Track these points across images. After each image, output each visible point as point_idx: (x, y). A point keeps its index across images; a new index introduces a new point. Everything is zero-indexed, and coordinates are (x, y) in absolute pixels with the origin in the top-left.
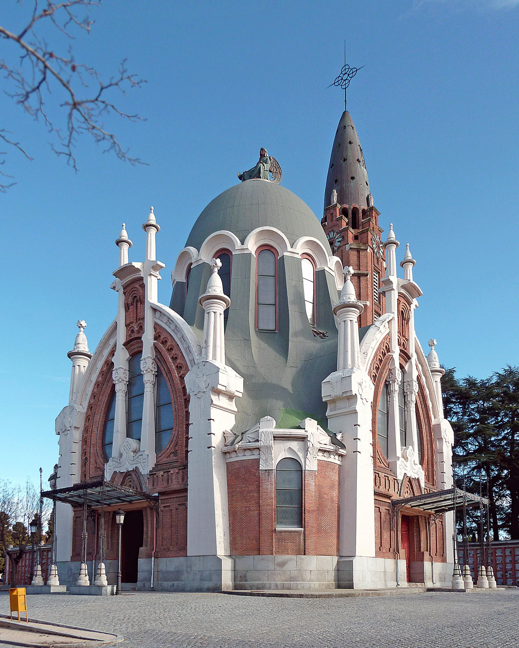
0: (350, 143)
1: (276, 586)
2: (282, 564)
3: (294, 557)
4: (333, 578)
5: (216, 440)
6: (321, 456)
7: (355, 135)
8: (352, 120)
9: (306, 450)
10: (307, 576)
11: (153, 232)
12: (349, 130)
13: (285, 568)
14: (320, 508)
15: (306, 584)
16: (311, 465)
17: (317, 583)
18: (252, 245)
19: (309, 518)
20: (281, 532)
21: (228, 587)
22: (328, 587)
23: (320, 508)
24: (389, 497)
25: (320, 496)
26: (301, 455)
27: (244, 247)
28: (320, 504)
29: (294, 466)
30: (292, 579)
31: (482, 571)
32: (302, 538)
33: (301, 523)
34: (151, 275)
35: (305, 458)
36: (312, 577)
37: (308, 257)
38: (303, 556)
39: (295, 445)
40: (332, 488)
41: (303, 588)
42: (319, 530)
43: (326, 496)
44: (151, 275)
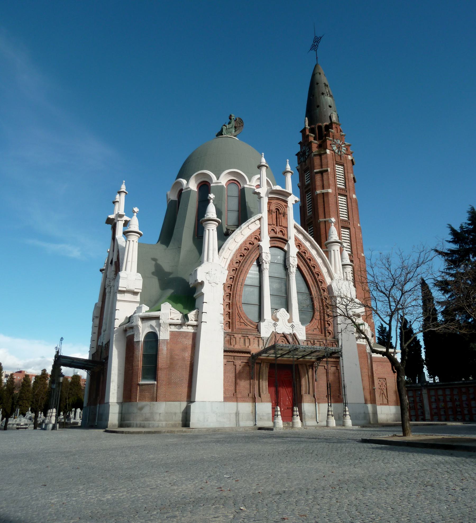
0: (317, 84)
1: (137, 425)
2: (141, 409)
3: (148, 403)
4: (180, 418)
5: (117, 324)
6: (174, 329)
7: (323, 79)
8: (321, 69)
9: (159, 325)
10: (157, 417)
11: (264, 169)
12: (318, 76)
13: (142, 412)
14: (171, 366)
15: (156, 423)
16: (164, 335)
17: (164, 423)
18: (223, 180)
19: (161, 374)
20: (142, 385)
21: (114, 426)
22: (174, 426)
23: (171, 366)
24: (249, 353)
25: (172, 357)
26: (157, 329)
27: (218, 181)
28: (171, 363)
29: (152, 338)
30: (147, 420)
31: (277, 411)
32: (155, 388)
33: (155, 378)
34: (118, 220)
35: (159, 331)
36: (161, 418)
37: (233, 182)
38: (155, 403)
39: (153, 323)
40: (184, 349)
41: (153, 427)
42: (169, 383)
43: (177, 357)
44: (118, 220)
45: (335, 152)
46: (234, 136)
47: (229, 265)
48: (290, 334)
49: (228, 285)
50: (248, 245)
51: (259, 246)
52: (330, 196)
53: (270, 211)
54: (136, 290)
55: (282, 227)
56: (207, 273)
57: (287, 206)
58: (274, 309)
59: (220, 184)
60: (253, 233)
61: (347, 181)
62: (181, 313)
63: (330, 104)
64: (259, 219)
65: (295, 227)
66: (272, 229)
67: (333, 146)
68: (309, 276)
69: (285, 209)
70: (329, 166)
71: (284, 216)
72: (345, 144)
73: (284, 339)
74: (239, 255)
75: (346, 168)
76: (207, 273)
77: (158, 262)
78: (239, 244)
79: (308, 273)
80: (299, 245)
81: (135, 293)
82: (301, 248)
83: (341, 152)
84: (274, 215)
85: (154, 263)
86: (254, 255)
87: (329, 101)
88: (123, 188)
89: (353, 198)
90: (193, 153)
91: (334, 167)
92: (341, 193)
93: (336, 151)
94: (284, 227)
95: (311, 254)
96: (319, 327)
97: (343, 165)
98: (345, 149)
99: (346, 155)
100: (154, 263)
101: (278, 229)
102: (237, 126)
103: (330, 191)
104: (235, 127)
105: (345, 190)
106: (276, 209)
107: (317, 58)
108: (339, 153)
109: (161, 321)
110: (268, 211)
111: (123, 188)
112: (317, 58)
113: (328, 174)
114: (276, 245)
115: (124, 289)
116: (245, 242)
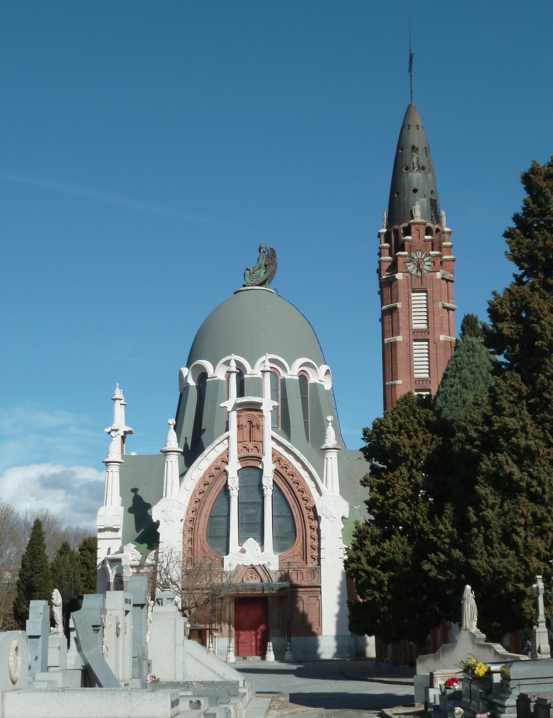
45: (411, 275)
46: (260, 285)
47: (191, 497)
48: (260, 565)
49: (190, 519)
50: (213, 471)
51: (225, 471)
52: (399, 347)
53: (239, 427)
54: (114, 527)
55: (255, 443)
56: (163, 511)
57: (262, 416)
58: (241, 540)
59: (215, 379)
60: (220, 455)
61: (431, 315)
62: (141, 554)
63: (415, 185)
64: (228, 438)
65: (273, 438)
66: (244, 447)
67: (408, 264)
68: (290, 495)
69: (259, 419)
70: (400, 298)
71: (258, 428)
72: (430, 255)
73: (254, 570)
74: (203, 484)
75: (430, 295)
76: (163, 511)
77: (138, 493)
78: (203, 472)
79: (289, 492)
80: (277, 459)
81: (116, 530)
82: (281, 463)
83: (421, 271)
84: (246, 429)
85: (133, 494)
86: (221, 481)
87: (415, 180)
88: (118, 393)
89: (439, 341)
90: (202, 326)
91: (409, 297)
92: (419, 338)
93: (414, 272)
94: (258, 442)
95: (294, 468)
96: (302, 553)
97: (426, 291)
98: (430, 263)
99: (432, 274)
100: (133, 494)
101: (251, 446)
102: (267, 263)
103: (399, 338)
104: (266, 266)
105: (426, 331)
106: (248, 421)
107: (412, 91)
108: (419, 274)
109: (123, 564)
110: (238, 426)
111: (118, 393)
112: (412, 91)
113: (398, 313)
114: (249, 465)
115: (103, 527)
116: (210, 468)
